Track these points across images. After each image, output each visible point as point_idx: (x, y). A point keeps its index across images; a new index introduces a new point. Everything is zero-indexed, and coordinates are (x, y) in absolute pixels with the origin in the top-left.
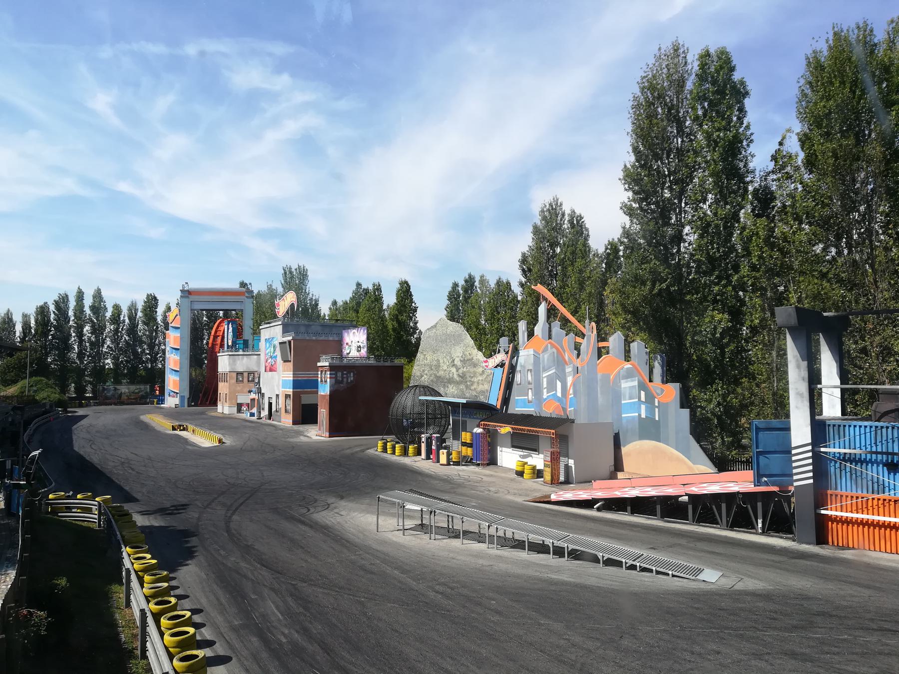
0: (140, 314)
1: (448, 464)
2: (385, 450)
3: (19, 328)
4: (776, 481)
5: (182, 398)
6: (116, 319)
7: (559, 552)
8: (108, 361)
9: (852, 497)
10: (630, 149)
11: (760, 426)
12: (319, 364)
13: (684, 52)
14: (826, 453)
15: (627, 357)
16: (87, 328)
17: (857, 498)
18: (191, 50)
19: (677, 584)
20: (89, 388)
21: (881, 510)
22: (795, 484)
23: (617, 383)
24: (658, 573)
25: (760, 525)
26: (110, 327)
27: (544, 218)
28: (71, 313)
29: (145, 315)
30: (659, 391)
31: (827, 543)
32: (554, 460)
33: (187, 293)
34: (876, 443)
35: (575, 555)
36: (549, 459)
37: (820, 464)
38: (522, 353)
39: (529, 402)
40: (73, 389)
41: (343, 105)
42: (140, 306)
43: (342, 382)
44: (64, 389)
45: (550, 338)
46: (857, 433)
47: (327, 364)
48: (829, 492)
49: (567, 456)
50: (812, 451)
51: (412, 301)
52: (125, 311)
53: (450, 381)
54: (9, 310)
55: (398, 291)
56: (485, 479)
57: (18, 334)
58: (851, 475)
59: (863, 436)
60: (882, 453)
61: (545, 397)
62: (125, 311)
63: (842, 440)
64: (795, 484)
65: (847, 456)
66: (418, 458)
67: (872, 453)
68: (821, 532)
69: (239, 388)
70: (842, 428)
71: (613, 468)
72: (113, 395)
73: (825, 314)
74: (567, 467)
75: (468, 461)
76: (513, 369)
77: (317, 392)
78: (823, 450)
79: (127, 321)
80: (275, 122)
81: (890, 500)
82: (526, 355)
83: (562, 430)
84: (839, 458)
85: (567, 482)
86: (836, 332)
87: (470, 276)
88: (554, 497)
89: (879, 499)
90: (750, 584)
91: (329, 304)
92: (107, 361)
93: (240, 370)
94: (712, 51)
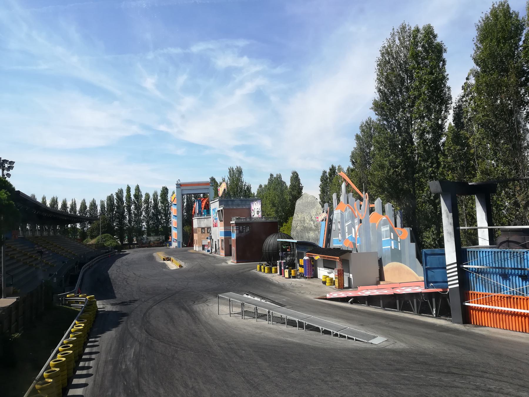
0: (159, 198)
1: (290, 277)
2: (260, 270)
3: (99, 208)
4: (439, 285)
5: (179, 243)
6: (147, 201)
7: (301, 325)
8: (144, 224)
9: (483, 295)
10: (376, 91)
11: (428, 252)
12: (231, 222)
13: (409, 29)
14: (467, 268)
15: (384, 211)
16: (133, 206)
17: (486, 295)
18: (197, 48)
19: (359, 345)
20: (135, 239)
21: (500, 303)
22: (450, 287)
23: (379, 228)
24: (349, 338)
25: (434, 312)
26: (144, 206)
27: (363, 131)
28: (124, 199)
29: (162, 198)
30: (400, 233)
31: (471, 323)
32: (340, 275)
33: (179, 186)
34: (495, 262)
35: (309, 328)
36: (337, 274)
37: (464, 276)
38: (335, 212)
39: (340, 241)
40: (127, 239)
41: (279, 70)
42: (159, 193)
43: (243, 232)
44: (122, 240)
45: (348, 203)
46: (484, 256)
47: (234, 222)
48: (470, 292)
49: (349, 272)
50: (457, 267)
51: (299, 183)
52: (151, 196)
53: (311, 229)
54: (84, 200)
55: (291, 178)
56: (304, 286)
57: (98, 211)
58: (482, 281)
59: (487, 257)
60: (499, 268)
61: (347, 237)
62: (151, 196)
63: (476, 259)
64: (450, 287)
65: (474, 269)
66: (276, 274)
67: (493, 268)
68: (466, 316)
69: (203, 237)
70: (475, 253)
71: (378, 279)
72: (146, 242)
73: (470, 184)
74: (349, 279)
75: (302, 276)
76: (330, 221)
77: (231, 238)
78: (465, 266)
79: (153, 202)
80: (241, 84)
81: (504, 297)
82: (337, 213)
83: (344, 256)
84: (475, 272)
85: (350, 287)
86: (486, 192)
87: (333, 166)
88: (328, 296)
89: (498, 296)
90: (400, 345)
91: (258, 187)
92: (143, 224)
93: (203, 226)
94: (421, 28)
